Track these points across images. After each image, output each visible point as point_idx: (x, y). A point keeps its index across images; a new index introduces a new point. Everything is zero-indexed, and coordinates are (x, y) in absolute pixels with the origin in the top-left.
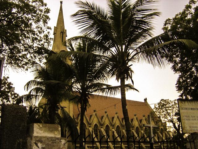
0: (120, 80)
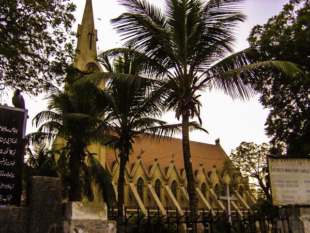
0: (181, 118)
